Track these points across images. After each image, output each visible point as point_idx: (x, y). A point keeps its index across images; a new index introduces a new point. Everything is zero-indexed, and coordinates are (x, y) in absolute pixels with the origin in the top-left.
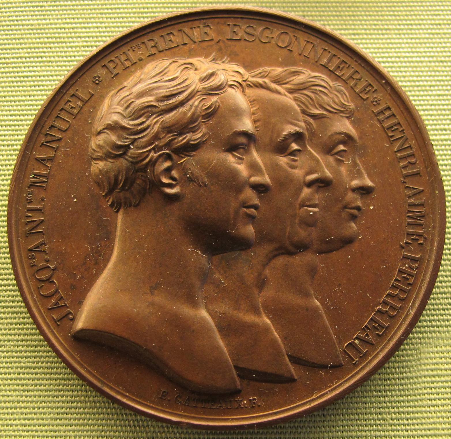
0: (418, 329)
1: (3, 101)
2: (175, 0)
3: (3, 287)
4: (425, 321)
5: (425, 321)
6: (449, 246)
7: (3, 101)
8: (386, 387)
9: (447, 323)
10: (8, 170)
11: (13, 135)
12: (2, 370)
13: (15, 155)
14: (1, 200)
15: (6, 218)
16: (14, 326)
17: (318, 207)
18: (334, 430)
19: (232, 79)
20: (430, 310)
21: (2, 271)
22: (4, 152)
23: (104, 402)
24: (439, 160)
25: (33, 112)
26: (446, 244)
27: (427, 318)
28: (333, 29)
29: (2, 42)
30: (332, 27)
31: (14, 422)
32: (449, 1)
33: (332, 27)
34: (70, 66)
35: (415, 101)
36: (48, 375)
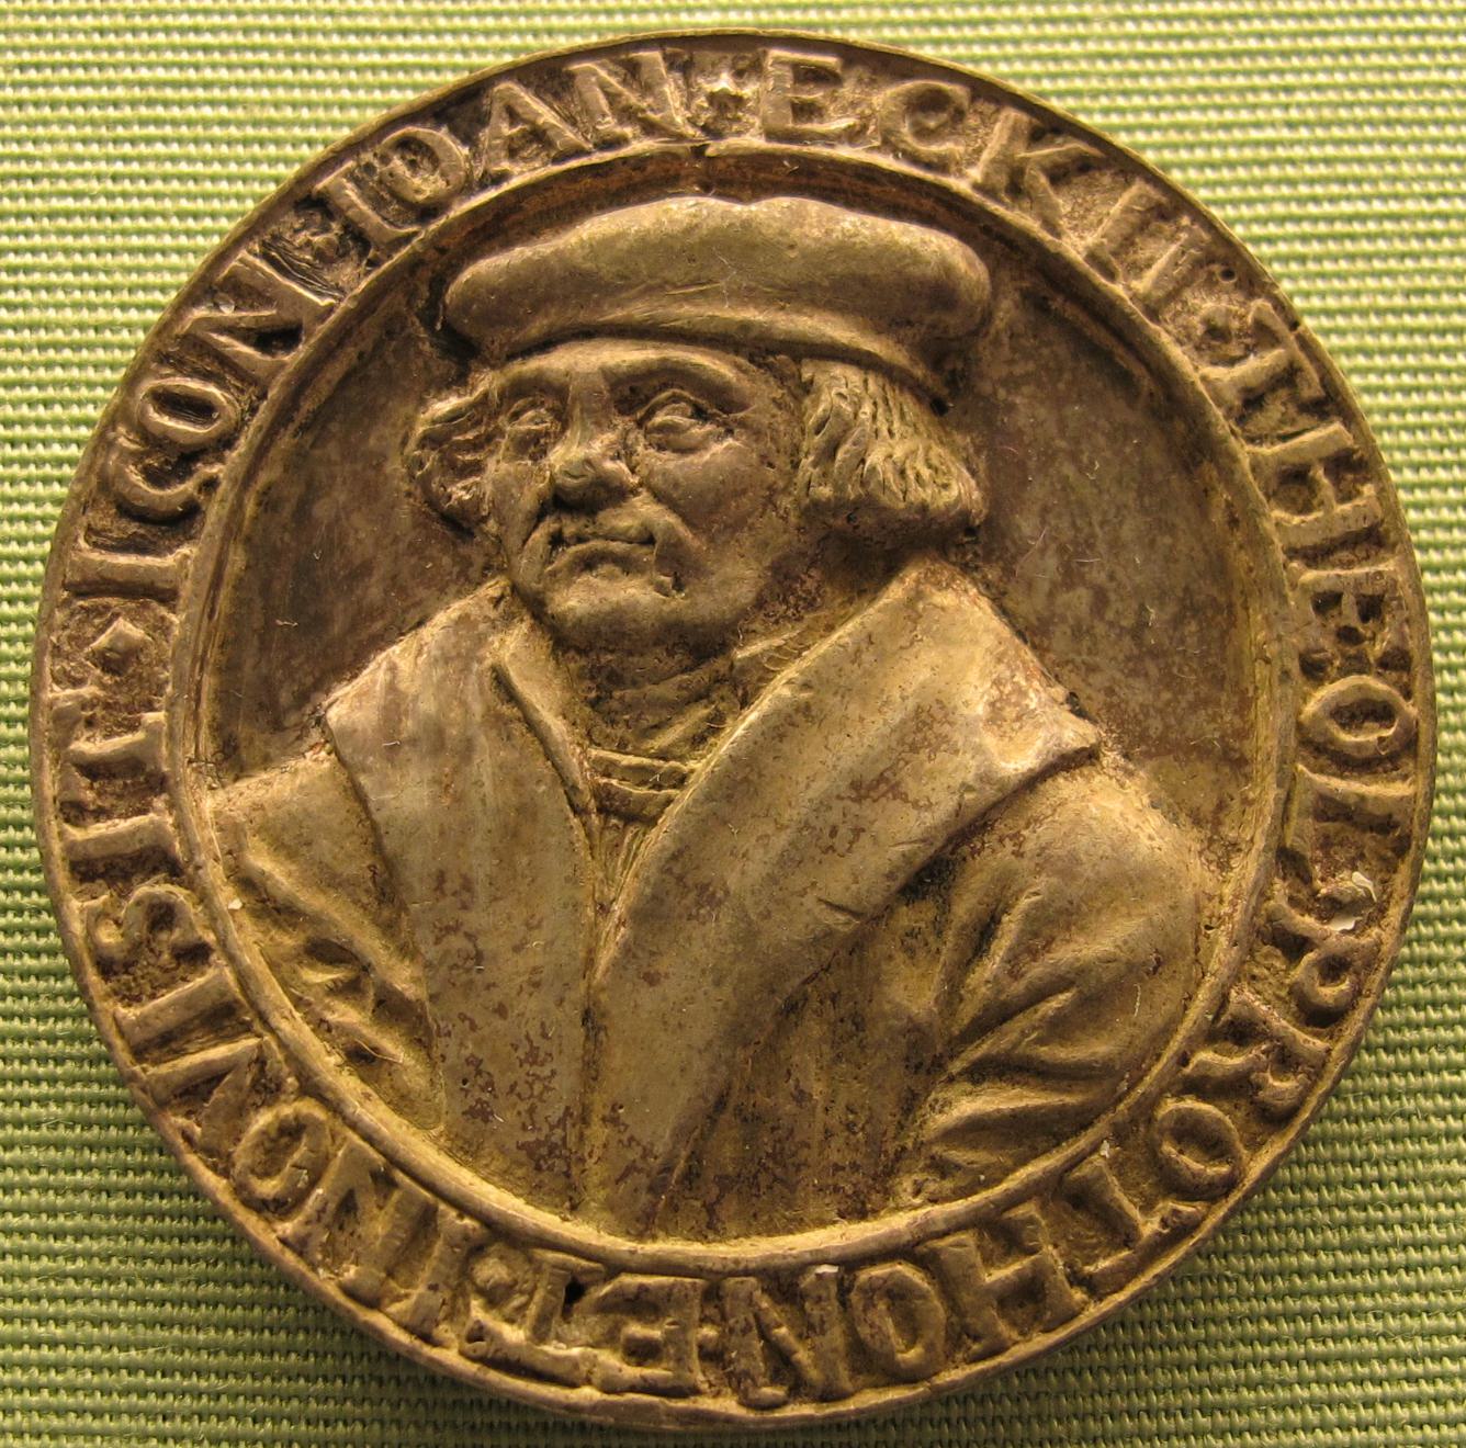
1: (13, 559)
2: (627, 1)
3: (11, 788)
7: (13, 559)
8: (1392, 1252)
11: (38, 1145)
13: (79, 443)
16: (61, 1087)
17: (989, 1290)
21: (6, 608)
22: (15, 469)
23: (398, 1423)
29: (6, 568)
31: (71, 1355)
32: (1455, 13)
33: (1192, 174)
34: (287, 162)
36: (239, 1310)
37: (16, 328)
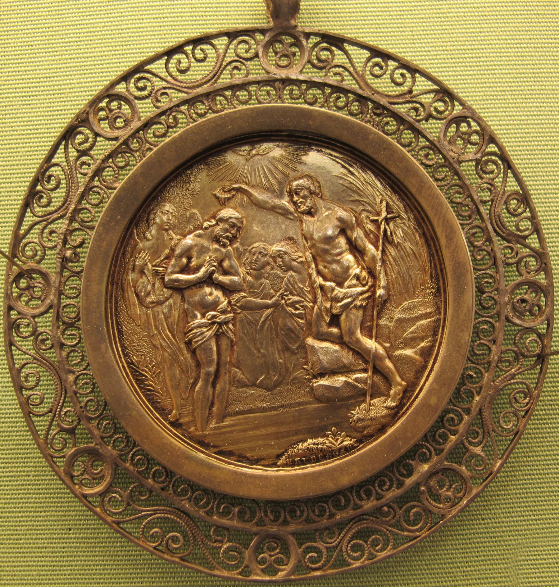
9: (556, 462)
10: (25, 182)
35: (493, 125)
37: (3, 149)
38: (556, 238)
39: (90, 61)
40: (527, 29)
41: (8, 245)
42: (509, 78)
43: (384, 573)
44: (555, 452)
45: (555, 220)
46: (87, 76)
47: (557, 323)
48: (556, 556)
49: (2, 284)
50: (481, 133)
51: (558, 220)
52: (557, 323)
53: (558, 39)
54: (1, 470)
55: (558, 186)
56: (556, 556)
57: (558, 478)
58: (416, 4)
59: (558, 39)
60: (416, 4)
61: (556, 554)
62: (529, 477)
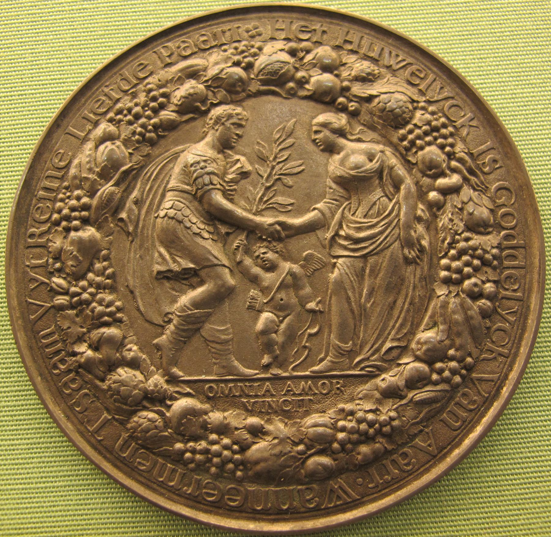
0: (517, 396)
4: (530, 372)
5: (530, 372)
6: (549, 296)
12: (2, 95)
14: (1, 303)
15: (6, 304)
18: (490, 257)
19: (211, 414)
20: (533, 363)
24: (531, 175)
25: (34, 142)
26: (546, 294)
27: (532, 370)
28: (381, 21)
30: (380, 19)
33: (380, 19)
38: (548, 471)
39: (184, 12)
40: (507, 54)
41: (6, 232)
42: (501, 53)
43: (385, 522)
44: (547, 398)
45: (547, 210)
46: (17, 89)
47: (548, 265)
48: (547, 443)
49: (2, 270)
50: (363, 438)
51: (550, 228)
52: (548, 265)
53: (550, 400)
54: (0, 458)
55: (550, 447)
56: (547, 443)
57: (549, 405)
58: (375, 4)
59: (550, 400)
60: (375, 4)
61: (548, 440)
62: (518, 466)
